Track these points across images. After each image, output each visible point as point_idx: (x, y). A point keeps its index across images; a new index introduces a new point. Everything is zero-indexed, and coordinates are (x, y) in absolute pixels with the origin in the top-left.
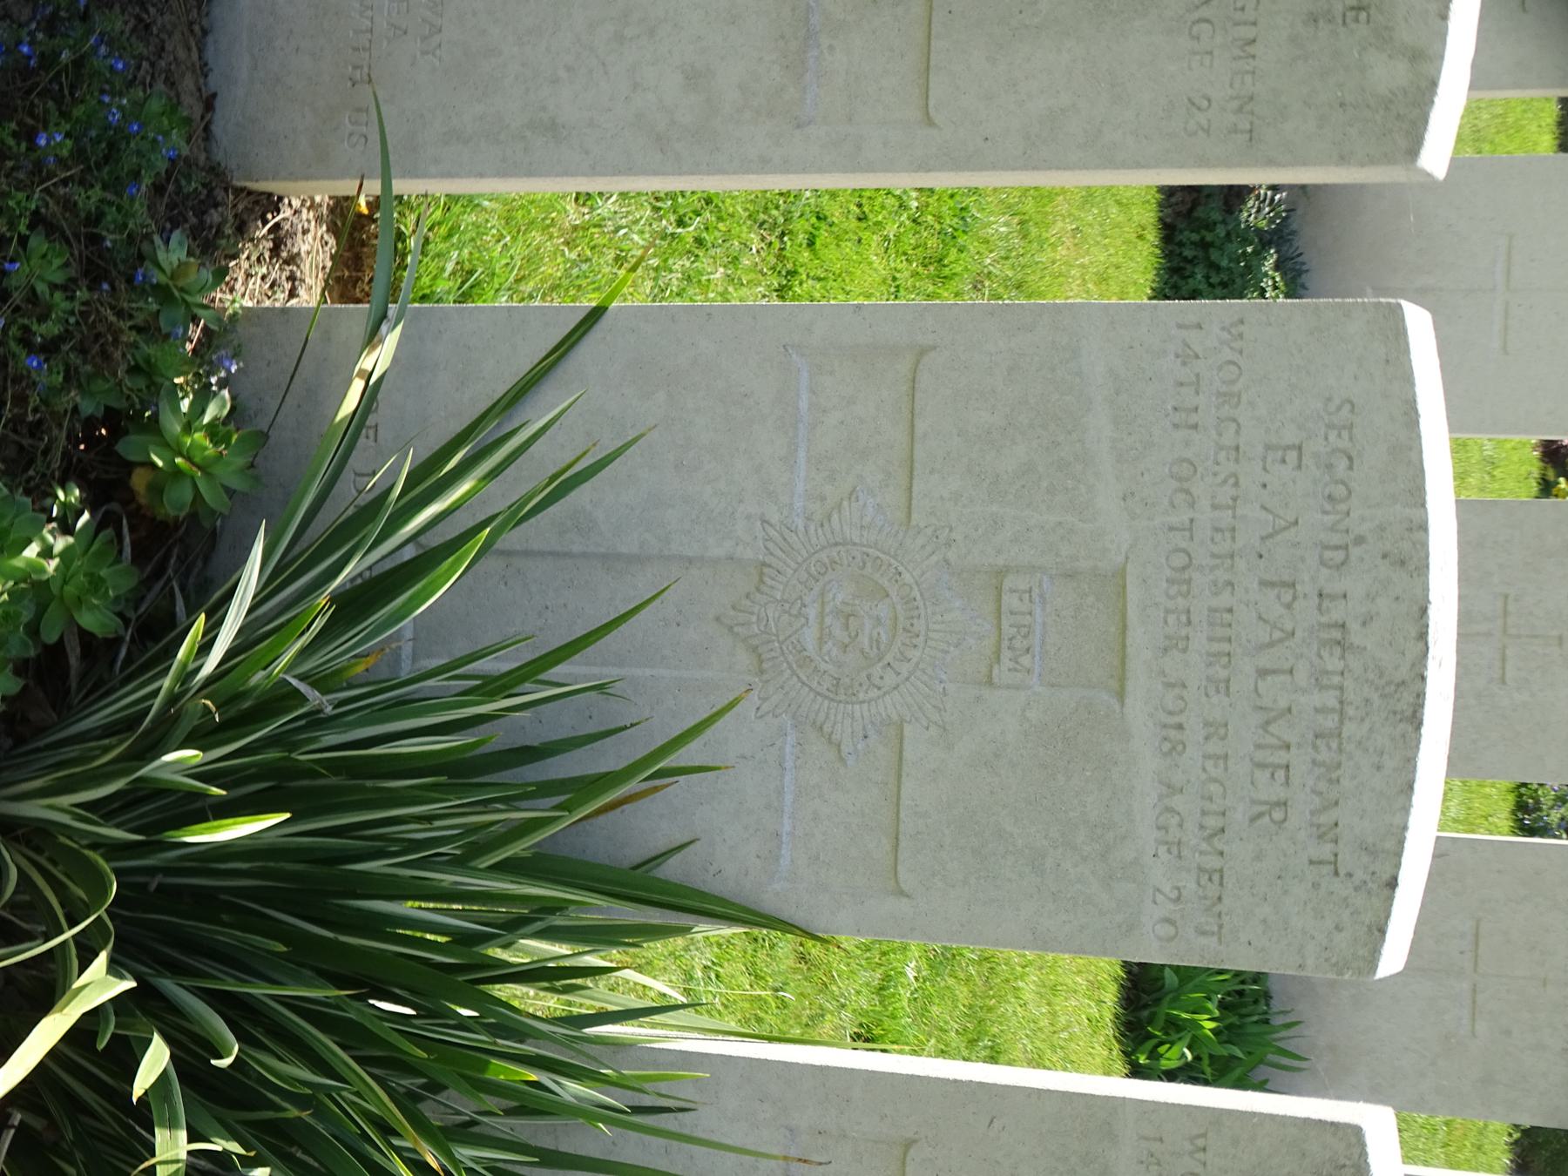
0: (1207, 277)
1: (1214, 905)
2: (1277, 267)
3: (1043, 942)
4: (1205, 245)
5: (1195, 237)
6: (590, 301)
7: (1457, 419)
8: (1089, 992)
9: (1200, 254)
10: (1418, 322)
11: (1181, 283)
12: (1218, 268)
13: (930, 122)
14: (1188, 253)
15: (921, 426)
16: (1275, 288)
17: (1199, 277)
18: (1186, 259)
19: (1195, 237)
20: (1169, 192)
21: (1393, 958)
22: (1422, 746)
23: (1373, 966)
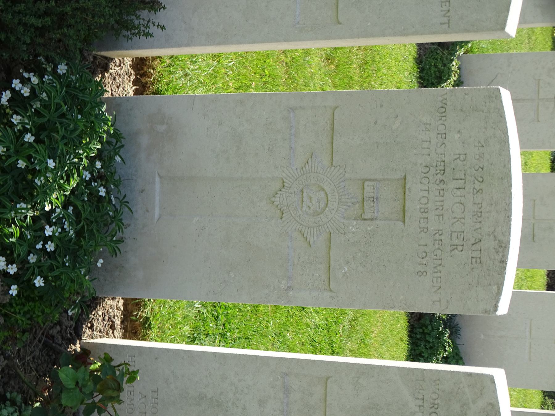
0: (425, 346)
1: (447, 13)
2: (449, 338)
3: (399, 92)
4: (424, 333)
5: (421, 330)
6: (283, 219)
7: (523, 144)
9: (423, 336)
10: (506, 95)
11: (416, 348)
12: (429, 342)
14: (418, 336)
16: (449, 346)
17: (422, 346)
18: (418, 339)
19: (421, 330)
20: (420, 46)
21: (503, 308)
22: (512, 233)
23: (496, 308)
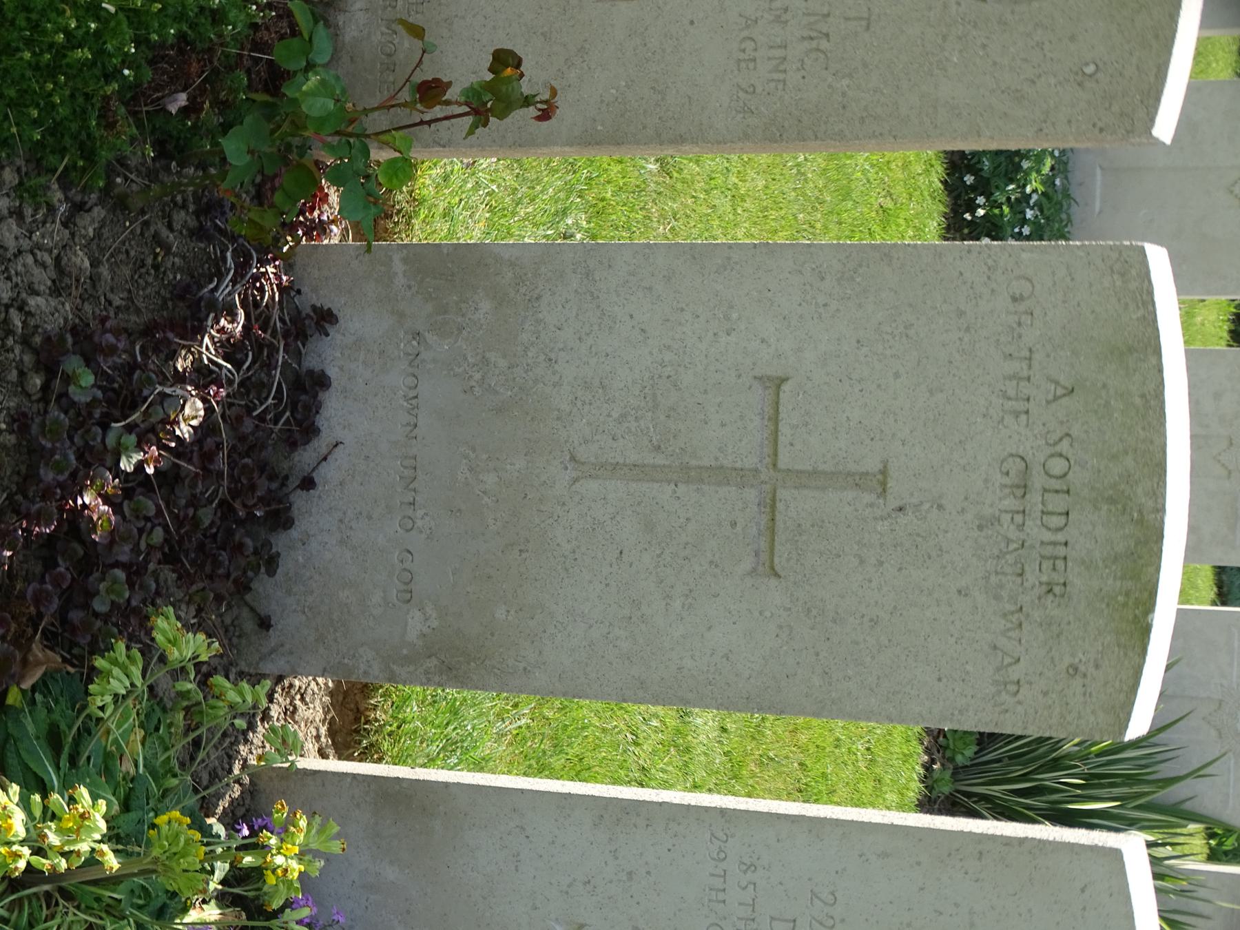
10: (1158, 259)
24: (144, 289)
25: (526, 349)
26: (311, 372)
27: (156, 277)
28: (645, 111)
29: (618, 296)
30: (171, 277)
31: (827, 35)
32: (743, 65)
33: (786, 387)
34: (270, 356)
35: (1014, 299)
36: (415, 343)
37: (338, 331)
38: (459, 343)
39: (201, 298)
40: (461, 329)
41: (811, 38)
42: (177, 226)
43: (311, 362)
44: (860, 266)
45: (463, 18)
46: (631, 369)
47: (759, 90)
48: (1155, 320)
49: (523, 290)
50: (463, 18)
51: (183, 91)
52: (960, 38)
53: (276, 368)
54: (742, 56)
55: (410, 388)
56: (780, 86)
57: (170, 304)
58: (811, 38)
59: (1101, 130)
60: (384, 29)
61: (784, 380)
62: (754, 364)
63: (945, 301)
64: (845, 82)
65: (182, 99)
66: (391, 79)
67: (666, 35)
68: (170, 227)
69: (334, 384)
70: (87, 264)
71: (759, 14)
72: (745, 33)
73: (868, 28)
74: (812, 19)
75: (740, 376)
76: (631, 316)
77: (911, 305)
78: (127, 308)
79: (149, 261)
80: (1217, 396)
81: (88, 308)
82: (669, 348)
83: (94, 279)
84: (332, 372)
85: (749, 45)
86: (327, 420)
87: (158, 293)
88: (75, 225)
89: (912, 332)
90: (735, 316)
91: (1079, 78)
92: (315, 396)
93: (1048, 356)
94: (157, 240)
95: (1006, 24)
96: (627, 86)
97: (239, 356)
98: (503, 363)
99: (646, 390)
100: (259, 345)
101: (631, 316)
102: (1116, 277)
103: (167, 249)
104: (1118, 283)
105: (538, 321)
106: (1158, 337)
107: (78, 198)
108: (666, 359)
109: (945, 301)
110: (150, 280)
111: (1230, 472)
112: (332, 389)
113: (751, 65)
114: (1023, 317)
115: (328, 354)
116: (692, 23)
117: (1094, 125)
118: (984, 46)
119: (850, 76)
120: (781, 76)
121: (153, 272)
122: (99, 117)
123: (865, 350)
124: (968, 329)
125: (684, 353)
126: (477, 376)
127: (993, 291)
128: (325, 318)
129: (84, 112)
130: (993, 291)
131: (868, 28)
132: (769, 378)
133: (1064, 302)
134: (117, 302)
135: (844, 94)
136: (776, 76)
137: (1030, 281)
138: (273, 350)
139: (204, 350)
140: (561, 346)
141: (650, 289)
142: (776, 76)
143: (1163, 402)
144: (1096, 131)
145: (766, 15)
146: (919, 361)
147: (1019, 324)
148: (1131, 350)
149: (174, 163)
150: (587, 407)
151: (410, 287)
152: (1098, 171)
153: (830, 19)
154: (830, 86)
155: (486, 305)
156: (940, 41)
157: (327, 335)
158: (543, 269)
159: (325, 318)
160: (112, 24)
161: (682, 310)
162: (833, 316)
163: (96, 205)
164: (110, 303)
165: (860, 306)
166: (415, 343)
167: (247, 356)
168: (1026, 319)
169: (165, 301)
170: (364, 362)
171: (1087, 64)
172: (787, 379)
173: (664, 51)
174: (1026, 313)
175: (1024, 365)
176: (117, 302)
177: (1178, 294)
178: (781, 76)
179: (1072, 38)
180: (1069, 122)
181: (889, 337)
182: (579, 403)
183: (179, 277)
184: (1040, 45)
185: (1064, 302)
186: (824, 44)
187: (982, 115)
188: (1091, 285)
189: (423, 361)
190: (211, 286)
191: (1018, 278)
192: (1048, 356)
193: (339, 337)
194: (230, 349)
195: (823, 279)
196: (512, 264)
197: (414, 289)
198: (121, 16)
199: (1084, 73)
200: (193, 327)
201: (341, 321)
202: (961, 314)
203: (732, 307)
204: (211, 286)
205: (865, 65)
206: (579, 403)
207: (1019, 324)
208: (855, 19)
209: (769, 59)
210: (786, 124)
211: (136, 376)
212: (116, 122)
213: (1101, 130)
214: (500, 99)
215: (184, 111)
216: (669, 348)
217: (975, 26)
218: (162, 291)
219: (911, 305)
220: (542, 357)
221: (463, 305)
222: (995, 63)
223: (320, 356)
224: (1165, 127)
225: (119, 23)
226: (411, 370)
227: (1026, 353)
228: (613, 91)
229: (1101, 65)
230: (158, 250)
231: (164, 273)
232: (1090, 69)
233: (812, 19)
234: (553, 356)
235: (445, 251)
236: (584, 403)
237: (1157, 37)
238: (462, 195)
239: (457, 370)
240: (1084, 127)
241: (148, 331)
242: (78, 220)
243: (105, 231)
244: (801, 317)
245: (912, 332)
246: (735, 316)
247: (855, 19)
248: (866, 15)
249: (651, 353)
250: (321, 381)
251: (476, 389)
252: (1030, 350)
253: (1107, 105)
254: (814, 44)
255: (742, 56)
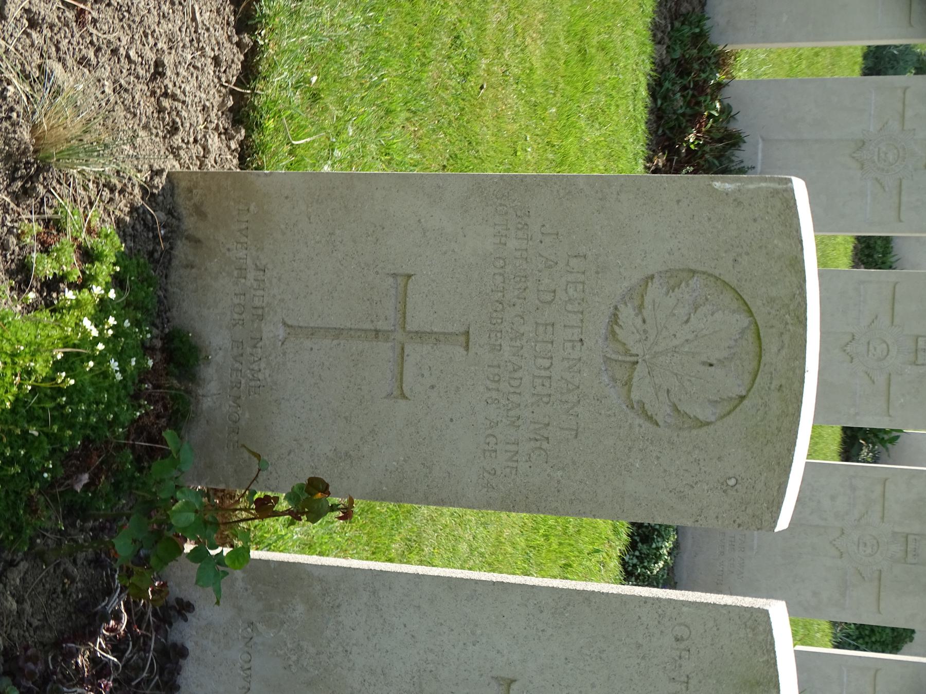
8: (611, 536)
10: (799, 187)
13: (879, 612)
15: (877, 689)
24: (55, 609)
25: (329, 642)
26: (174, 645)
27: (64, 598)
28: (417, 480)
29: (396, 609)
30: (75, 597)
31: (547, 439)
32: (487, 454)
33: (514, 686)
34: (145, 644)
35: (677, 640)
36: (249, 630)
37: (194, 616)
38: (281, 633)
39: (96, 613)
40: (283, 623)
41: (537, 440)
42: (79, 562)
43: (175, 635)
44: (568, 605)
45: (288, 400)
46: (404, 663)
47: (499, 473)
48: (775, 664)
49: (328, 599)
50: (288, 400)
51: (85, 472)
52: (641, 450)
53: (149, 652)
54: (487, 447)
55: (246, 662)
56: (514, 472)
57: (74, 616)
58: (537, 440)
59: (739, 525)
60: (231, 402)
61: (513, 681)
62: (492, 668)
63: (628, 636)
64: (560, 473)
65: (85, 478)
66: (236, 439)
67: (433, 427)
68: (75, 562)
69: (191, 654)
70: (15, 606)
71: (499, 419)
72: (489, 432)
73: (576, 437)
74: (537, 426)
75: (482, 675)
76: (405, 626)
77: (603, 636)
78: (43, 626)
79: (59, 589)
80: (833, 498)
81: (15, 632)
82: (431, 651)
83: (20, 613)
84: (190, 645)
85: (492, 440)
86: (185, 679)
87: (66, 609)
88: (7, 578)
89: (604, 656)
90: (479, 632)
91: (725, 488)
92: (177, 663)
93: (700, 682)
94: (66, 574)
95: (673, 443)
96: (405, 460)
97: (122, 647)
98: (312, 650)
99: (415, 679)
100: (136, 638)
101: (405, 626)
102: (748, 630)
103: (73, 581)
104: (750, 635)
105: (338, 623)
106: (778, 676)
107: (9, 558)
108: (429, 659)
109: (628, 636)
110: (59, 601)
111: (842, 554)
112: (189, 658)
113: (493, 455)
114: (683, 653)
115: (187, 633)
116: (452, 420)
117: (734, 521)
118: (658, 458)
119: (563, 469)
120: (515, 465)
121: (61, 596)
122: (26, 505)
123: (570, 665)
124: (644, 658)
125: (443, 655)
126: (294, 658)
127: (662, 632)
128: (184, 608)
129: (14, 503)
130: (662, 632)
131: (576, 437)
132: (503, 679)
133: (712, 645)
134: (36, 623)
135: (559, 482)
136: (510, 464)
137: (689, 628)
138: (147, 638)
139: (97, 648)
140: (354, 642)
141: (419, 607)
142: (510, 464)
143: (805, 298)
144: (736, 525)
145: (504, 420)
146: (609, 677)
147: (680, 657)
148: (758, 683)
149: (78, 521)
150: (372, 687)
151: (247, 590)
152: (760, 140)
153: (550, 428)
154: (549, 475)
155: (301, 608)
156: (626, 451)
157: (186, 620)
158: (342, 586)
159: (184, 608)
160: (36, 444)
161: (441, 624)
162: (548, 639)
163: (22, 560)
164: (31, 625)
165: (568, 634)
166: (249, 630)
167: (128, 645)
168: (685, 654)
169: (70, 614)
170: (213, 640)
171: (730, 478)
172: (515, 681)
173: (431, 438)
174: (685, 650)
175: (683, 687)
176: (36, 623)
177: (815, 231)
178: (515, 465)
179: (719, 458)
180: (717, 517)
181: (588, 658)
182: (366, 684)
183: (80, 596)
184: (697, 461)
185: (712, 645)
186: (545, 445)
187: (656, 507)
188: (731, 635)
189: (255, 643)
190: (103, 604)
191: (680, 624)
192: (700, 682)
193: (194, 620)
194: (116, 646)
195: (542, 612)
196: (320, 580)
197: (250, 591)
198: (43, 438)
199: (728, 485)
200: (90, 632)
201: (197, 609)
202: (639, 646)
203: (477, 626)
204: (103, 604)
205: (574, 463)
206: (366, 684)
207: (680, 657)
208: (567, 429)
209: (506, 451)
210: (517, 499)
211: (48, 688)
212: (37, 510)
213: (739, 525)
214: (310, 501)
215: (87, 487)
216: (431, 651)
217: (652, 443)
218: (68, 608)
219: (603, 636)
220: (340, 649)
221: (285, 606)
222: (665, 471)
223: (181, 633)
224: (783, 522)
225: (41, 443)
226: (246, 649)
227: (684, 679)
228: (395, 463)
229: (739, 479)
230: (66, 581)
231: (70, 595)
232: (732, 482)
233: (537, 426)
234: (348, 648)
235: (272, 566)
236: (370, 685)
237: (779, 463)
238: (282, 545)
239: (279, 651)
240: (727, 522)
241: (57, 645)
242: (9, 574)
243: (29, 578)
244: (526, 637)
245: (604, 656)
246: (479, 632)
247: (567, 429)
248: (575, 427)
249: (418, 653)
250: (181, 652)
251: (293, 667)
252: (688, 677)
253: (743, 508)
254: (538, 444)
255: (487, 447)
